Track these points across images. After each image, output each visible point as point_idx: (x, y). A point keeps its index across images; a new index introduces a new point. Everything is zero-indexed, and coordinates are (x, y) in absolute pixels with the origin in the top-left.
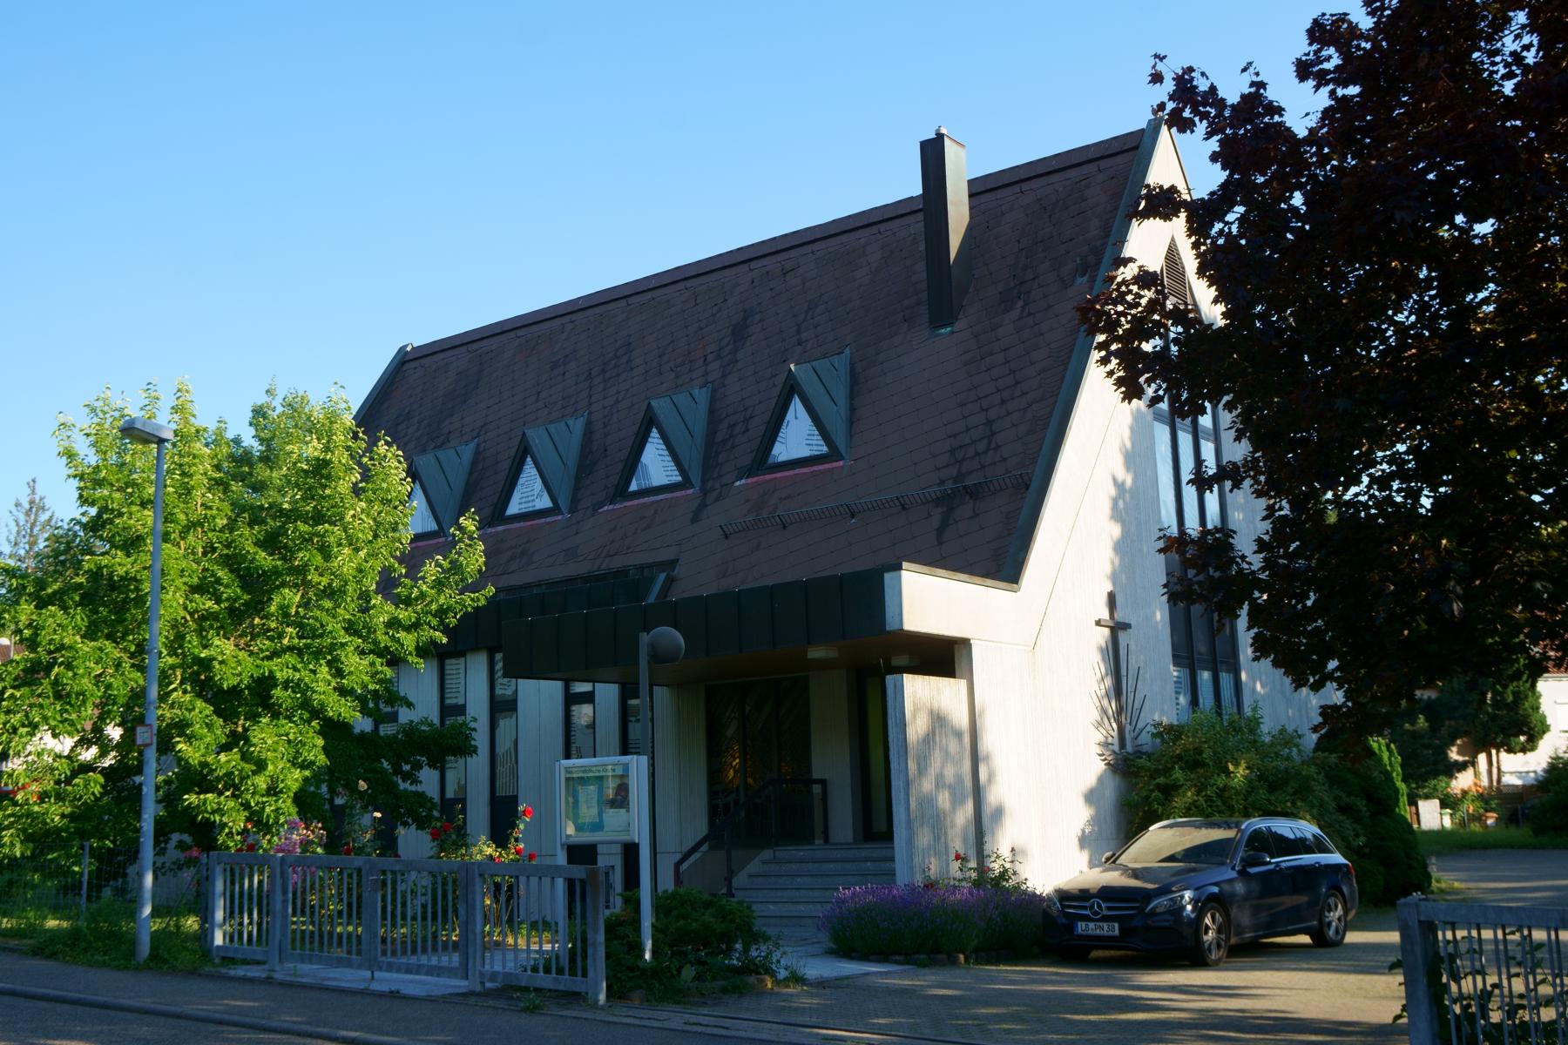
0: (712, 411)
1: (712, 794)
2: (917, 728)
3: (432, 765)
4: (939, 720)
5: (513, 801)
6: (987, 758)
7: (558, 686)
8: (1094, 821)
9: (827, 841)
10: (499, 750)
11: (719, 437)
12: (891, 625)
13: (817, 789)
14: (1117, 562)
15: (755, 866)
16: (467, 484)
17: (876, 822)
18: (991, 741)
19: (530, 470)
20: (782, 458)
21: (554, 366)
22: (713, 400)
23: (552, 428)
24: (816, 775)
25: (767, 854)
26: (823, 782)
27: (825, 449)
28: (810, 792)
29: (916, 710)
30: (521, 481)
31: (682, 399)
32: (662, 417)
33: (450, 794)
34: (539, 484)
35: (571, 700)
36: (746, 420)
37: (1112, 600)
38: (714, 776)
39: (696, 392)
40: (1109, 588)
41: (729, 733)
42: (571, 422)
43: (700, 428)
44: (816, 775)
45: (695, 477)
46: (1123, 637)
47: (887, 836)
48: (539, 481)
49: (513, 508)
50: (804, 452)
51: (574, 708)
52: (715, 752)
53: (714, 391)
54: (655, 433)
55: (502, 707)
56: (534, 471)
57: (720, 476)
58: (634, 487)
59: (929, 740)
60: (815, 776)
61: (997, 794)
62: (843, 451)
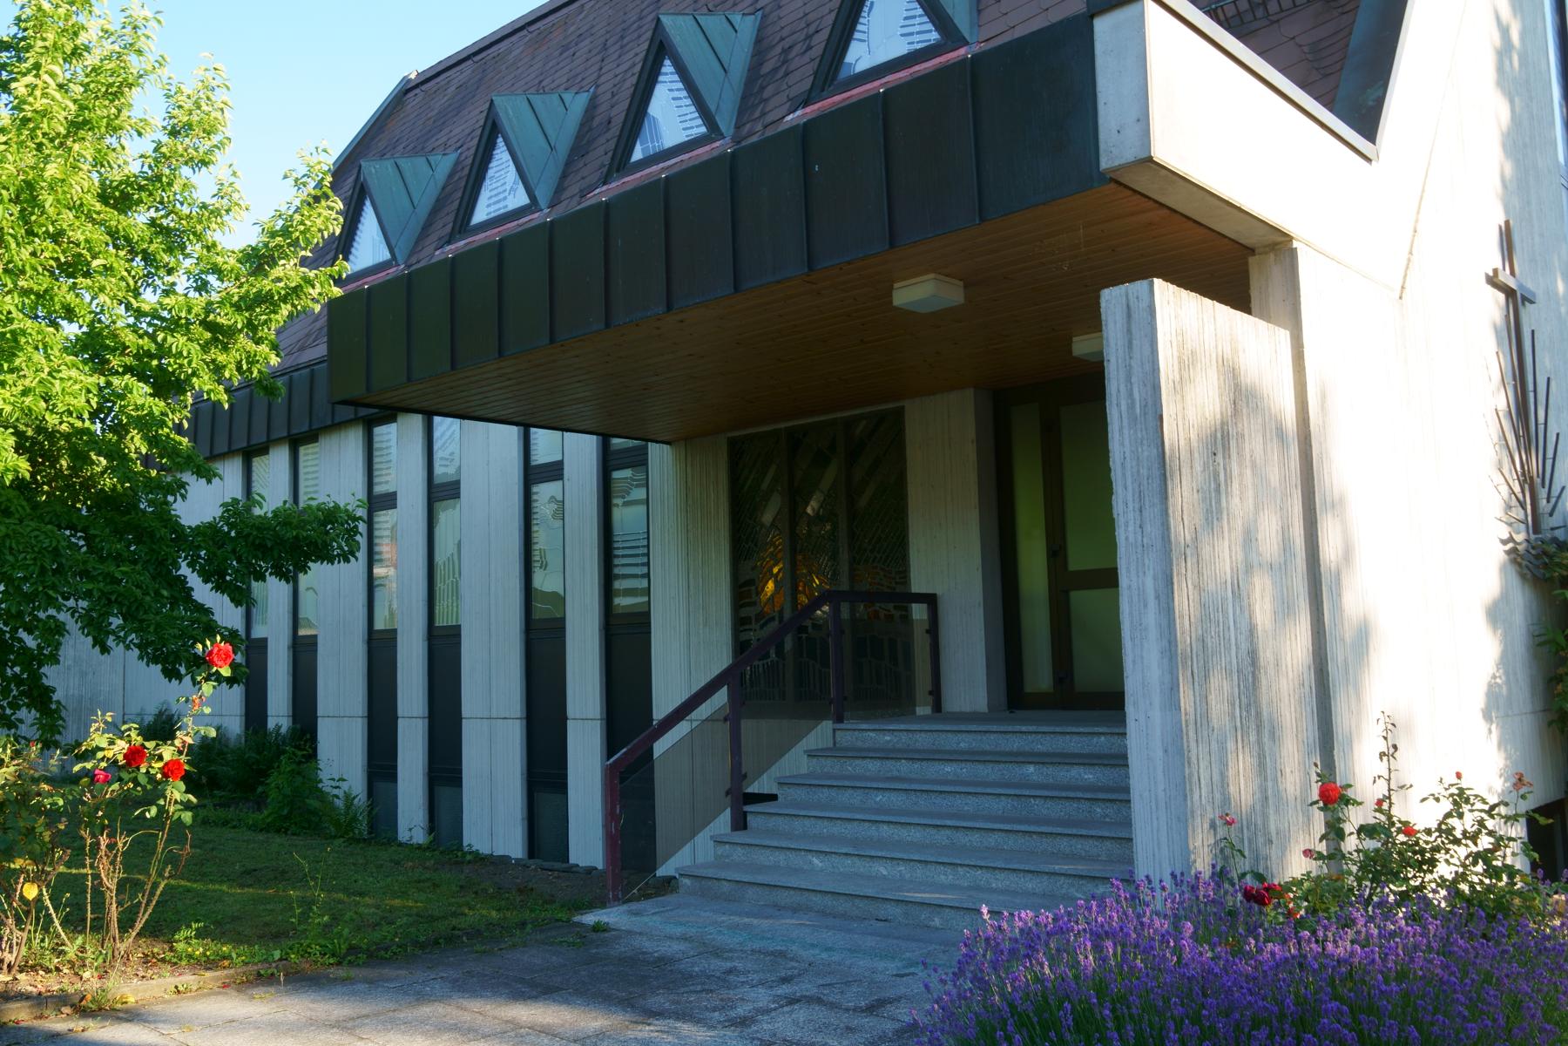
0: (758, 41)
1: (740, 623)
2: (1189, 408)
3: (281, 574)
4: (1242, 396)
5: (454, 634)
6: (1337, 505)
7: (511, 433)
8: (1504, 661)
9: (937, 707)
10: (440, 558)
11: (767, 68)
12: (1113, 152)
13: (919, 612)
14: (1509, 169)
15: (795, 762)
16: (438, 200)
17: (1066, 674)
18: (1341, 468)
19: (501, 156)
20: (861, 66)
21: (566, 48)
22: (761, 28)
23: (537, 100)
24: (918, 586)
25: (822, 733)
26: (931, 600)
27: (934, 36)
28: (906, 618)
29: (1187, 363)
30: (490, 173)
31: (713, 23)
32: (682, 49)
33: (379, 625)
34: (511, 173)
35: (534, 474)
36: (809, 37)
37: (1507, 240)
38: (743, 591)
39: (737, 19)
40: (1500, 219)
41: (767, 518)
42: (567, 97)
43: (739, 60)
44: (918, 586)
45: (726, 124)
46: (1529, 315)
47: (1108, 702)
48: (512, 168)
49: (481, 214)
50: (900, 48)
51: (535, 489)
52: (744, 545)
53: (764, 16)
54: (668, 67)
55: (440, 492)
56: (506, 156)
57: (763, 114)
58: (638, 154)
59: (1220, 442)
60: (916, 588)
61: (1363, 593)
62: (967, 36)
